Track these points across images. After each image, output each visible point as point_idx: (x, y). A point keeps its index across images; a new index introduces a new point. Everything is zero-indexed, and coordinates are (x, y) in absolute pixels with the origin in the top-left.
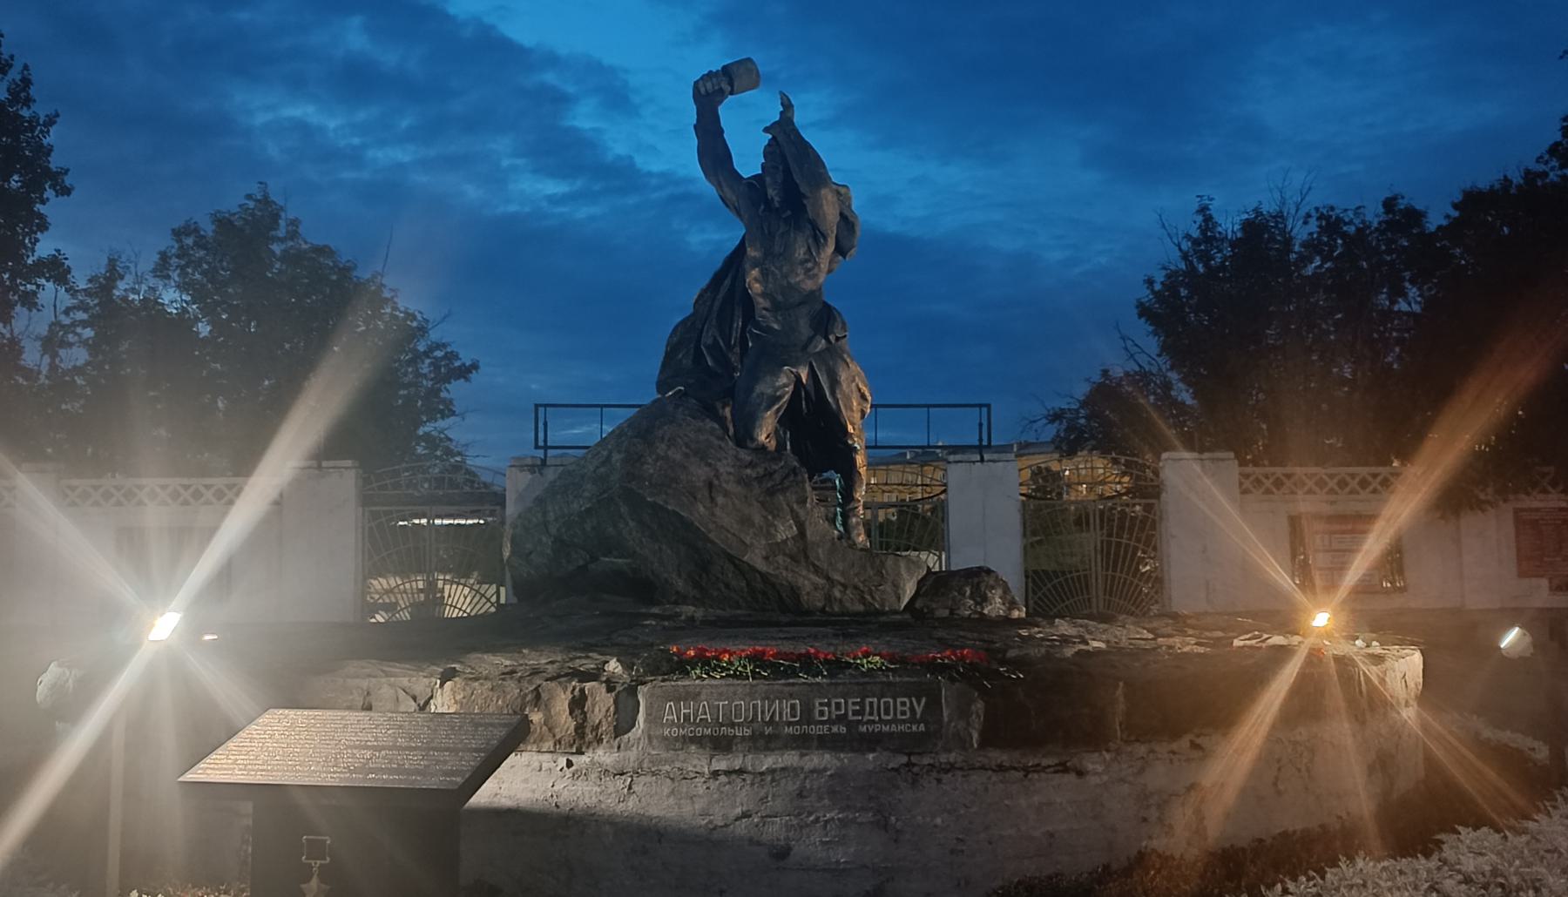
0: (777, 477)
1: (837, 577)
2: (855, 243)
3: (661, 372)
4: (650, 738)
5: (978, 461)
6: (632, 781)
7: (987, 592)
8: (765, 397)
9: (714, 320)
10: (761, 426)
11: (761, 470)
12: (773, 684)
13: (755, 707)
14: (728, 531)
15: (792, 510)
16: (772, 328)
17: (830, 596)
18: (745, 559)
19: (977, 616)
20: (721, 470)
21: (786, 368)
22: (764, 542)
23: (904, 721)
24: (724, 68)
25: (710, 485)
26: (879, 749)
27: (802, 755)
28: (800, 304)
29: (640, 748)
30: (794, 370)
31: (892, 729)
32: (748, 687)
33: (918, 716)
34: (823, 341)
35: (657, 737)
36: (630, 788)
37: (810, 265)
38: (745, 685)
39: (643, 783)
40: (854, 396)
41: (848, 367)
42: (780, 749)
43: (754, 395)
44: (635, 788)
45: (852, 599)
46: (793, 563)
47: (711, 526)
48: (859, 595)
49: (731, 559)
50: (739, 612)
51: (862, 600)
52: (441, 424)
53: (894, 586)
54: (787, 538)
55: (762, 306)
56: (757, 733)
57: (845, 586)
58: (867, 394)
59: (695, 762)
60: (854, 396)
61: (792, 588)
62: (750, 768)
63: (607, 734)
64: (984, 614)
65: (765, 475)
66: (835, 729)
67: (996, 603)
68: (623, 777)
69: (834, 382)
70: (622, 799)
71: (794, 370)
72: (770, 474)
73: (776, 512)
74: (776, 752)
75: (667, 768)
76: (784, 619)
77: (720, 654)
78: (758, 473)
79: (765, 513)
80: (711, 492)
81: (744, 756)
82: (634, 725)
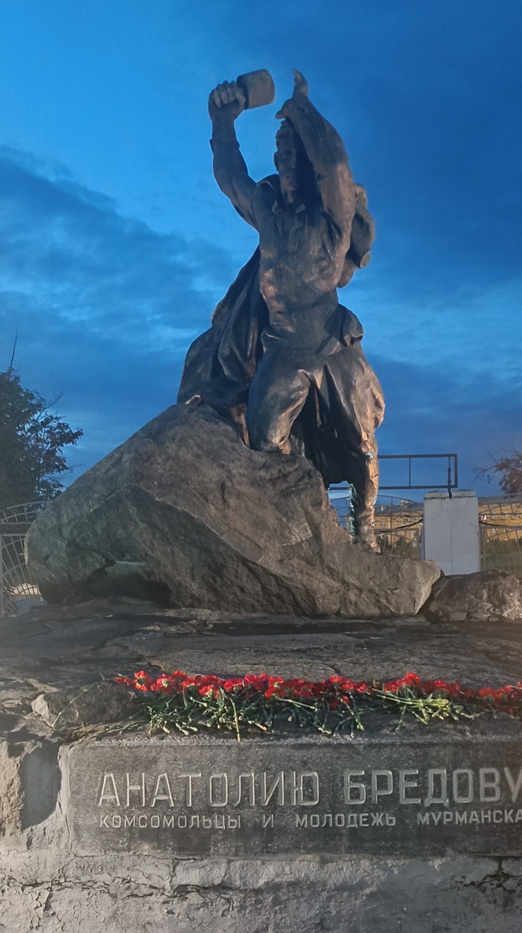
0: (292, 479)
1: (352, 580)
2: (370, 246)
3: (182, 386)
4: (77, 828)
5: (447, 498)
6: (50, 896)
7: (505, 594)
8: (279, 399)
9: (231, 331)
10: (275, 428)
11: (275, 472)
12: (275, 746)
13: (245, 783)
14: (241, 534)
15: (307, 513)
16: (286, 331)
17: (345, 599)
18: (259, 562)
19: (495, 619)
20: (234, 471)
21: (300, 371)
22: (277, 545)
23: (492, 806)
24: (240, 78)
25: (223, 487)
26: (449, 851)
27: (324, 862)
28: (315, 304)
29: (62, 847)
30: (308, 373)
31: (471, 820)
32: (234, 750)
33: (514, 798)
34: (338, 343)
35: (88, 829)
36: (48, 907)
37: (324, 263)
38: (229, 748)
39: (67, 900)
40: (369, 401)
41: (363, 370)
42: (287, 851)
43: (269, 396)
44: (55, 907)
45: (368, 603)
46: (308, 566)
47: (224, 528)
48: (375, 599)
49: (245, 562)
50: (254, 615)
51: (378, 603)
52: (56, 474)
53: (410, 589)
54: (302, 541)
55: (276, 309)
56: (250, 825)
57: (361, 590)
58: (382, 401)
59: (150, 870)
60: (369, 401)
61: (307, 591)
62: (238, 883)
63: (10, 822)
64: (504, 617)
65: (279, 478)
66: (377, 820)
67: (515, 606)
68: (37, 890)
69: (349, 388)
70: (35, 925)
71: (308, 373)
72: (285, 477)
73: (290, 514)
74: (281, 856)
75: (105, 877)
76: (299, 622)
77: (201, 687)
78: (272, 475)
79: (279, 515)
80: (223, 494)
81: (229, 862)
82: (52, 809)
